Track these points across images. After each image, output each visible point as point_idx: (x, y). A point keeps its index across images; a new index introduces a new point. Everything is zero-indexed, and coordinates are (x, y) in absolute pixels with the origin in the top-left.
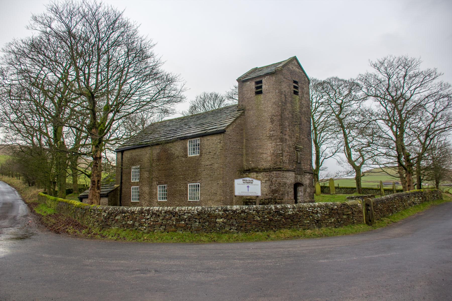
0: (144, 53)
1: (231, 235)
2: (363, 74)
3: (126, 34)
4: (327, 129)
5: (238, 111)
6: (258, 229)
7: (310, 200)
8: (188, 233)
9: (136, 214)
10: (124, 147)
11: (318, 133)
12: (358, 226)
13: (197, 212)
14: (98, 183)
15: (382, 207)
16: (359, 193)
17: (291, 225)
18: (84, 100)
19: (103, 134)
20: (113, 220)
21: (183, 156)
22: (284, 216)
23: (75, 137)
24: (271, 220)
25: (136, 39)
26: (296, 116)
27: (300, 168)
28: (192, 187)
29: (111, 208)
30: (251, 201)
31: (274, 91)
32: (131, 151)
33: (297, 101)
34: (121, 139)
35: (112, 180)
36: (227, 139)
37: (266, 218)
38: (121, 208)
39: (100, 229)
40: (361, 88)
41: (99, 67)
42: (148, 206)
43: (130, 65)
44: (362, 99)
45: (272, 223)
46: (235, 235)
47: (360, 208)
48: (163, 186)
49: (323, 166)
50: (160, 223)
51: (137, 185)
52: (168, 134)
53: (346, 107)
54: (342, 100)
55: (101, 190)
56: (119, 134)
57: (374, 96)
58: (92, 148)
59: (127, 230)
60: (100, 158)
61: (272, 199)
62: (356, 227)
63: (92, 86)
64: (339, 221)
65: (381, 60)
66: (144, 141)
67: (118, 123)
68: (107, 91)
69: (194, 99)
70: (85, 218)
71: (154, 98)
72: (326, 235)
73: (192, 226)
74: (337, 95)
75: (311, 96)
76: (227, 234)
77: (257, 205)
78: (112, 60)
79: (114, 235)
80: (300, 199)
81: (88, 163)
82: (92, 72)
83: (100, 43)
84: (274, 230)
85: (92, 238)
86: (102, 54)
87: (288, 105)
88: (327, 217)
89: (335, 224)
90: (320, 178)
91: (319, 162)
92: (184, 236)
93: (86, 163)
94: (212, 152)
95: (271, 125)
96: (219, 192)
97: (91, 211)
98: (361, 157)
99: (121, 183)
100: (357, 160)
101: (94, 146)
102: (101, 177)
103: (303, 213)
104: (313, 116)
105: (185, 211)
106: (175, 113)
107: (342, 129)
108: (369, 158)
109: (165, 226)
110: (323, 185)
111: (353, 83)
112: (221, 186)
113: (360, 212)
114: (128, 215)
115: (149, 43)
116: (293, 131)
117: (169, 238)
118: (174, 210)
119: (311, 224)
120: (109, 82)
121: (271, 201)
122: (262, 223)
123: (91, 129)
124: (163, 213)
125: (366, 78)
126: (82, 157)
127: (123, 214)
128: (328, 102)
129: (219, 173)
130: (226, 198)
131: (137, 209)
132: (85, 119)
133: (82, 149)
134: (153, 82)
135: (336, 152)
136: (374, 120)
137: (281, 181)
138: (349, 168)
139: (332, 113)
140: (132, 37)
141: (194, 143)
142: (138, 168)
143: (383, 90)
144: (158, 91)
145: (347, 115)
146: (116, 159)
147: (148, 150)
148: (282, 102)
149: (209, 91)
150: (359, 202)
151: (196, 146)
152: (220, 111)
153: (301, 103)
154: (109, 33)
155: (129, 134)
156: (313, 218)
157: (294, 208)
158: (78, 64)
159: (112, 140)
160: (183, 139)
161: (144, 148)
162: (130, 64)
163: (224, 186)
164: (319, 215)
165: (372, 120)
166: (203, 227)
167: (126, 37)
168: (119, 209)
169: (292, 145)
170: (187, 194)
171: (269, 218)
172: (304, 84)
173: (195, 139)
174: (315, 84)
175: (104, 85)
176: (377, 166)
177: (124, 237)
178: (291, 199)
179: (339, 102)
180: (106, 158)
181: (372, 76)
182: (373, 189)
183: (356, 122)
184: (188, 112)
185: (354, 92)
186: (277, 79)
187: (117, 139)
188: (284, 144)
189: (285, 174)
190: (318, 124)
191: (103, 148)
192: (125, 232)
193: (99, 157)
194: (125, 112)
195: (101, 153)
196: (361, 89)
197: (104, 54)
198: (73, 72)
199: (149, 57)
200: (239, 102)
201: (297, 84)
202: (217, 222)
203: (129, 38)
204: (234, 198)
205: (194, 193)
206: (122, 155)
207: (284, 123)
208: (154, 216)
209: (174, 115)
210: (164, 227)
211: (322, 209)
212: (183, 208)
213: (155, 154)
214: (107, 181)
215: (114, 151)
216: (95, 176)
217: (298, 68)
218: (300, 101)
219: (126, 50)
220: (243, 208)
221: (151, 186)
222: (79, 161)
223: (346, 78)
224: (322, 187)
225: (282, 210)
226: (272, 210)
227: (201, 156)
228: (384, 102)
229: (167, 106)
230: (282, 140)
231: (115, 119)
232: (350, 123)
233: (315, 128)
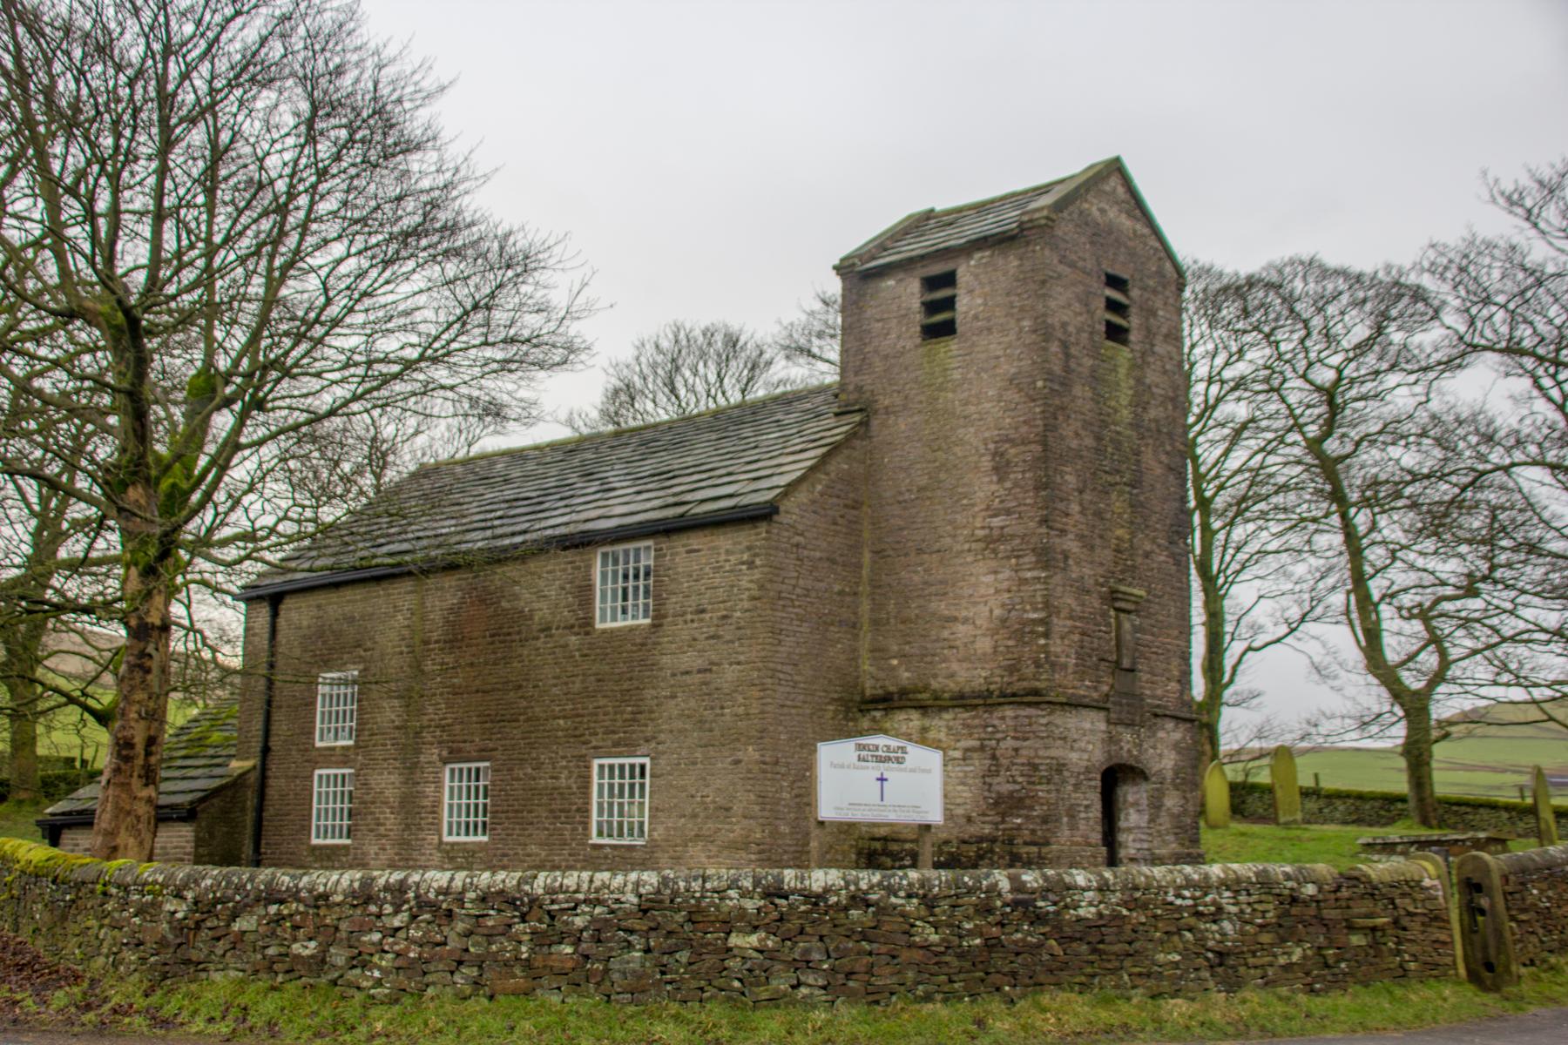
0: (392, 126)
1: (796, 1014)
2: (1452, 242)
3: (302, 31)
4: (1262, 506)
5: (837, 415)
6: (931, 988)
7: (1179, 849)
8: (589, 1002)
9: (338, 904)
10: (289, 576)
11: (1216, 525)
12: (1428, 993)
13: (635, 900)
14: (148, 754)
15: (1549, 899)
16: (1425, 822)
17: (1089, 970)
18: (86, 345)
19: (185, 513)
20: (218, 939)
21: (572, 626)
22: (1058, 927)
23: (34, 522)
24: (991, 945)
25: (354, 58)
26: (1118, 445)
27: (1134, 695)
28: (611, 776)
29: (212, 875)
30: (895, 847)
31: (1012, 323)
32: (320, 598)
33: (1122, 371)
34: (267, 538)
35: (216, 737)
36: (785, 550)
37: (971, 934)
38: (264, 874)
39: (146, 984)
40: (1437, 311)
41: (169, 184)
42: (393, 866)
43: (319, 182)
44: (1439, 363)
45: (998, 960)
46: (820, 1016)
47: (1436, 898)
48: (469, 770)
49: (1242, 684)
50: (450, 952)
51: (344, 763)
52: (500, 518)
53: (1360, 405)
54: (1339, 371)
55: (164, 787)
56: (259, 512)
57: (1501, 351)
58: (124, 582)
59: (288, 986)
60: (165, 628)
61: (993, 840)
62: (1419, 995)
63: (126, 275)
64: (1331, 962)
65: (1547, 174)
66: (385, 549)
67: (255, 458)
68: (210, 303)
69: (627, 355)
70: (73, 928)
71: (436, 345)
72: (1263, 1028)
73: (611, 966)
74: (1315, 345)
75: (1186, 350)
76: (778, 1007)
77: (924, 867)
78: (234, 154)
79: (217, 1014)
80: (1130, 843)
81: (95, 653)
82: (131, 207)
83: (172, 65)
84: (1006, 994)
85: (101, 1029)
86: (181, 121)
87: (1078, 390)
88: (1266, 938)
89: (1307, 974)
90: (1227, 744)
91: (1221, 664)
92: (572, 1018)
93: (88, 650)
94: (713, 611)
95: (994, 487)
96: (744, 800)
97: (105, 894)
98: (1432, 648)
99: (266, 750)
100: (1412, 657)
101: (134, 571)
102: (163, 722)
103: (1149, 913)
104: (1194, 444)
105: (577, 891)
106: (538, 419)
107: (1334, 507)
108: (1475, 652)
109: (480, 967)
110: (1240, 778)
111: (1396, 283)
112: (749, 771)
113: (1436, 918)
114: (298, 912)
115: (417, 77)
116: (1099, 514)
117: (496, 1024)
118: (527, 888)
119: (1187, 971)
120: (217, 262)
121: (992, 851)
122: (947, 959)
123: (124, 485)
124: (472, 901)
125: (1465, 262)
126: (65, 623)
127: (273, 909)
128: (1267, 380)
129: (741, 710)
130: (775, 834)
131: (345, 882)
132: (89, 436)
133: (70, 584)
134: (437, 268)
135: (1302, 620)
136: (1498, 468)
137: (1041, 753)
138: (1374, 697)
139: (1290, 430)
140: (331, 45)
141: (627, 562)
142: (354, 682)
143: (1550, 322)
144: (459, 311)
145: (1362, 440)
146: (240, 631)
147: (402, 595)
148: (1050, 377)
149: (697, 319)
150: (1429, 871)
151: (636, 577)
152: (750, 415)
153: (1139, 381)
154: (218, 18)
155: (309, 513)
156: (1201, 940)
157: (1103, 888)
158: (56, 166)
159: (224, 543)
160: (576, 546)
161: (385, 584)
162: (322, 174)
163: (765, 772)
164: (1227, 925)
165: (1489, 467)
166: (663, 973)
167: (301, 45)
168: (251, 879)
169: (1097, 583)
170: (585, 811)
171: (981, 935)
172: (1155, 292)
173: (631, 546)
174: (1205, 290)
175: (188, 276)
176: (1517, 694)
177: (271, 1025)
178: (1090, 845)
179: (1325, 376)
180: (191, 629)
181: (1496, 252)
182: (1493, 806)
183: (1409, 478)
184: (595, 414)
185: (1400, 329)
186: (1028, 265)
187: (249, 536)
188: (1058, 579)
189: (1059, 721)
190: (1217, 482)
191: (179, 579)
192: (276, 995)
193: (158, 622)
194: (290, 408)
195: (167, 604)
196: (1436, 315)
197: (193, 122)
198: (29, 201)
199: (418, 147)
200: (843, 373)
202: (729, 950)
203: (317, 47)
204: (815, 832)
205: (621, 805)
206: (275, 614)
207: (1058, 479)
208: (427, 916)
209: (533, 429)
210: (475, 972)
211: (1243, 898)
212: (571, 880)
213: (436, 616)
214: (193, 740)
215: (235, 597)
216: (134, 715)
217: (1129, 214)
218: (1137, 373)
219: (305, 107)
220: (856, 884)
221: (411, 769)
222: (50, 640)
223: (1365, 261)
224: (1234, 788)
225: (1044, 899)
226: (1000, 895)
227: (656, 626)
228: (1553, 376)
229: (501, 387)
230: (1046, 558)
231: (243, 440)
232: (1375, 483)
233: (1204, 504)
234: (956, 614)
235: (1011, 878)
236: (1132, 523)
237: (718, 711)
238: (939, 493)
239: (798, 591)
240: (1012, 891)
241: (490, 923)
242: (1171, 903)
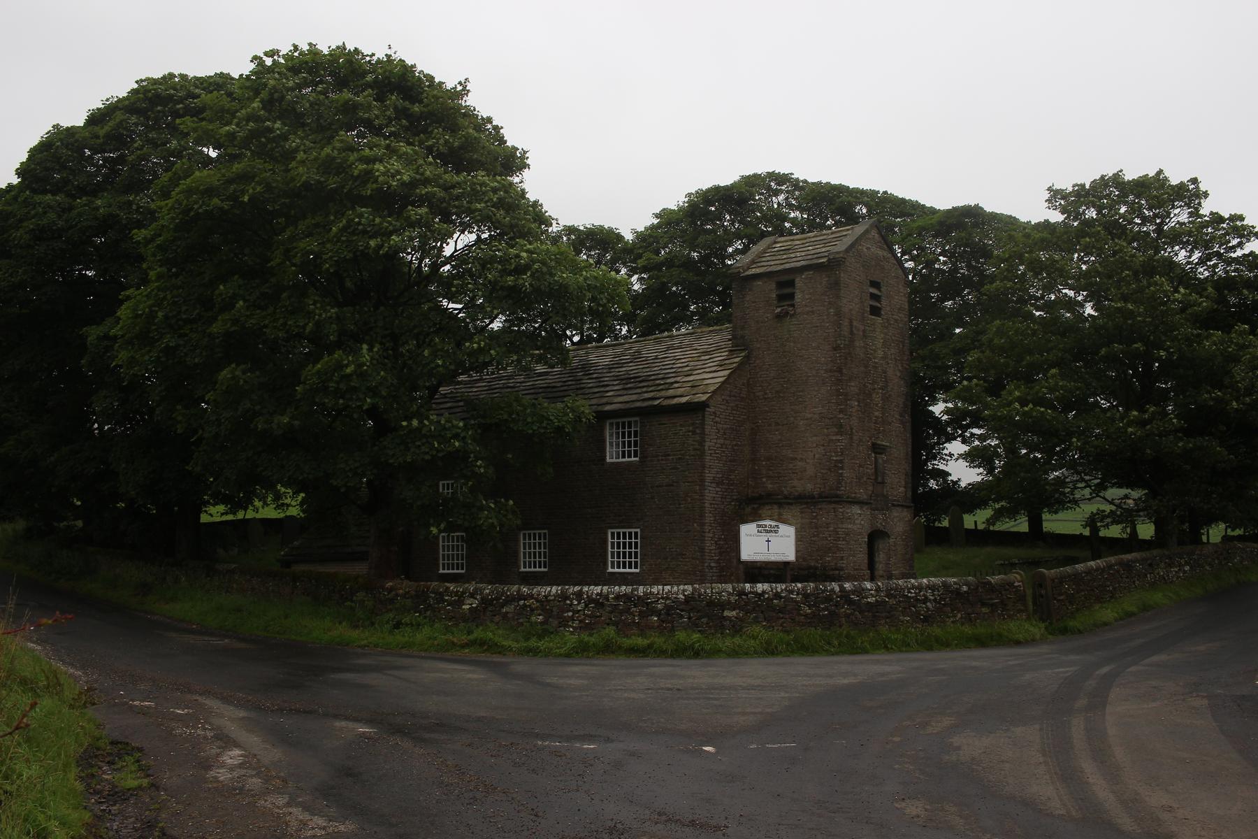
37: (824, 609)
47: (1020, 590)
94: (674, 455)
118: (636, 593)
124: (612, 598)
127: (522, 602)
201: (879, 301)
202: (724, 617)
212: (655, 590)
220: (776, 589)
225: (853, 595)
227: (644, 458)
234: (796, 456)
235: (839, 585)
236: (883, 408)
239: (717, 445)
240: (840, 591)
241: (621, 608)
242: (907, 595)
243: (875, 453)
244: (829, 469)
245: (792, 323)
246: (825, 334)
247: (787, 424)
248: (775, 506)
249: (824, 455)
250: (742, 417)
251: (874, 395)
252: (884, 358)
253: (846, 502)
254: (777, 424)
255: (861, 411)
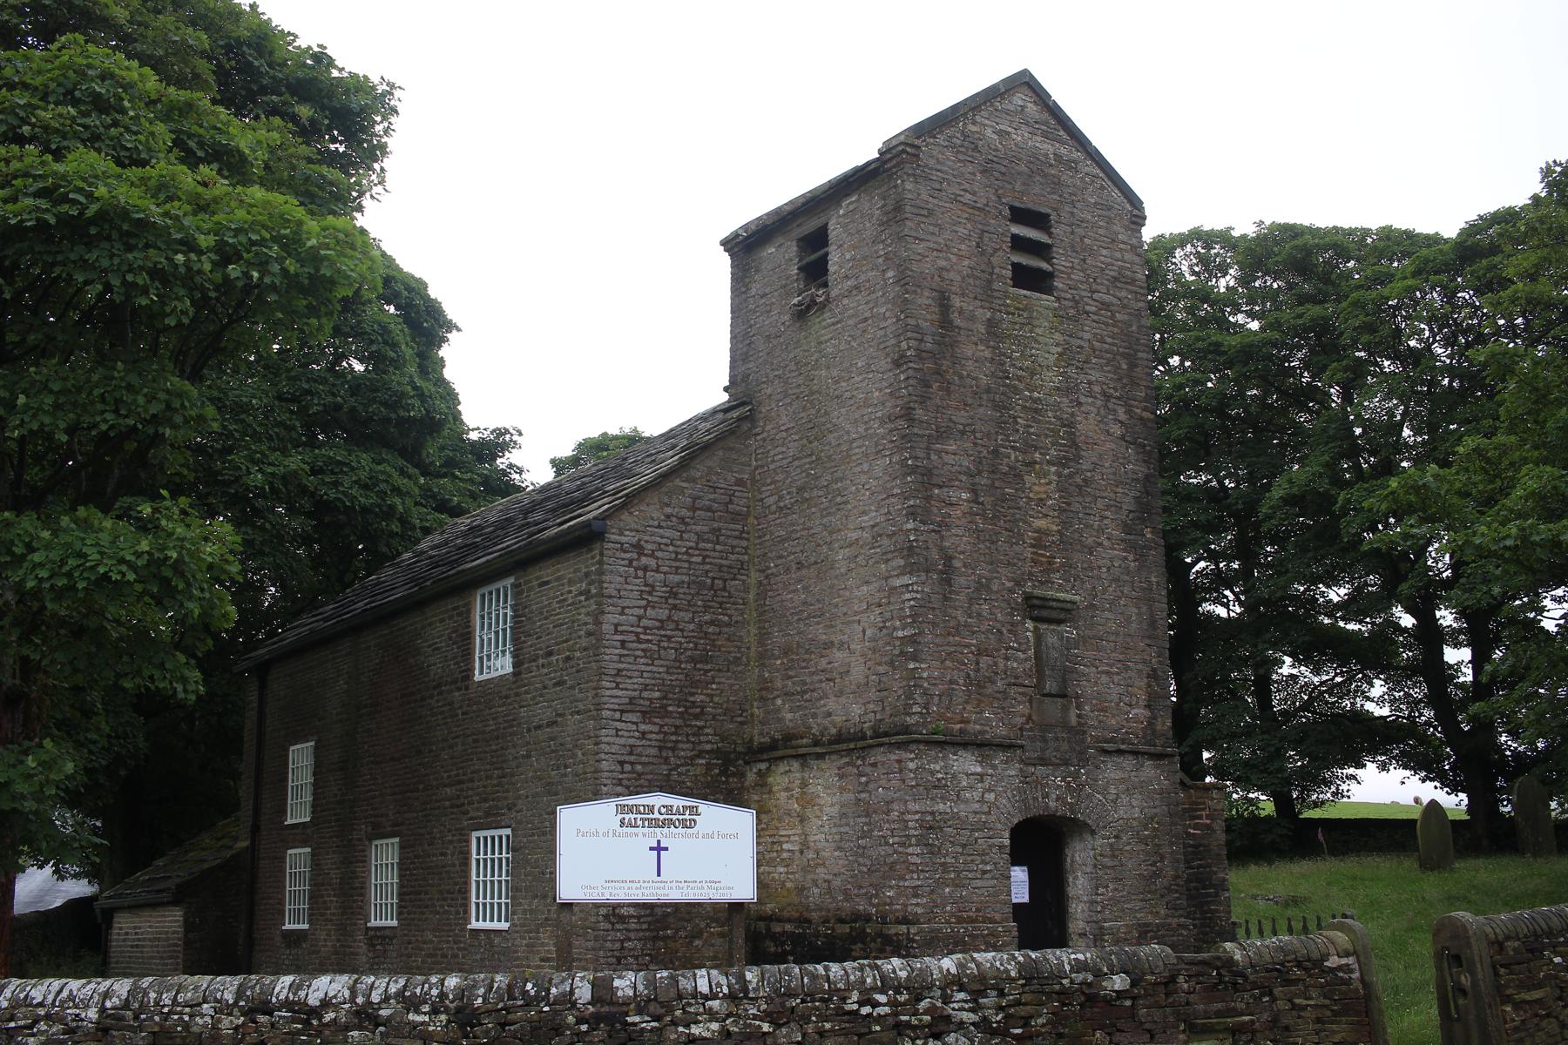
47: (1348, 982)
225: (639, 1012)
237: (562, 771)
238: (815, 493)
240: (593, 1002)
243: (1035, 619)
244: (891, 663)
245: (824, 323)
246: (882, 333)
247: (816, 563)
248: (796, 765)
249: (881, 629)
250: (733, 557)
251: (1030, 479)
252: (1068, 389)
253: (927, 743)
254: (800, 565)
255: (984, 516)
